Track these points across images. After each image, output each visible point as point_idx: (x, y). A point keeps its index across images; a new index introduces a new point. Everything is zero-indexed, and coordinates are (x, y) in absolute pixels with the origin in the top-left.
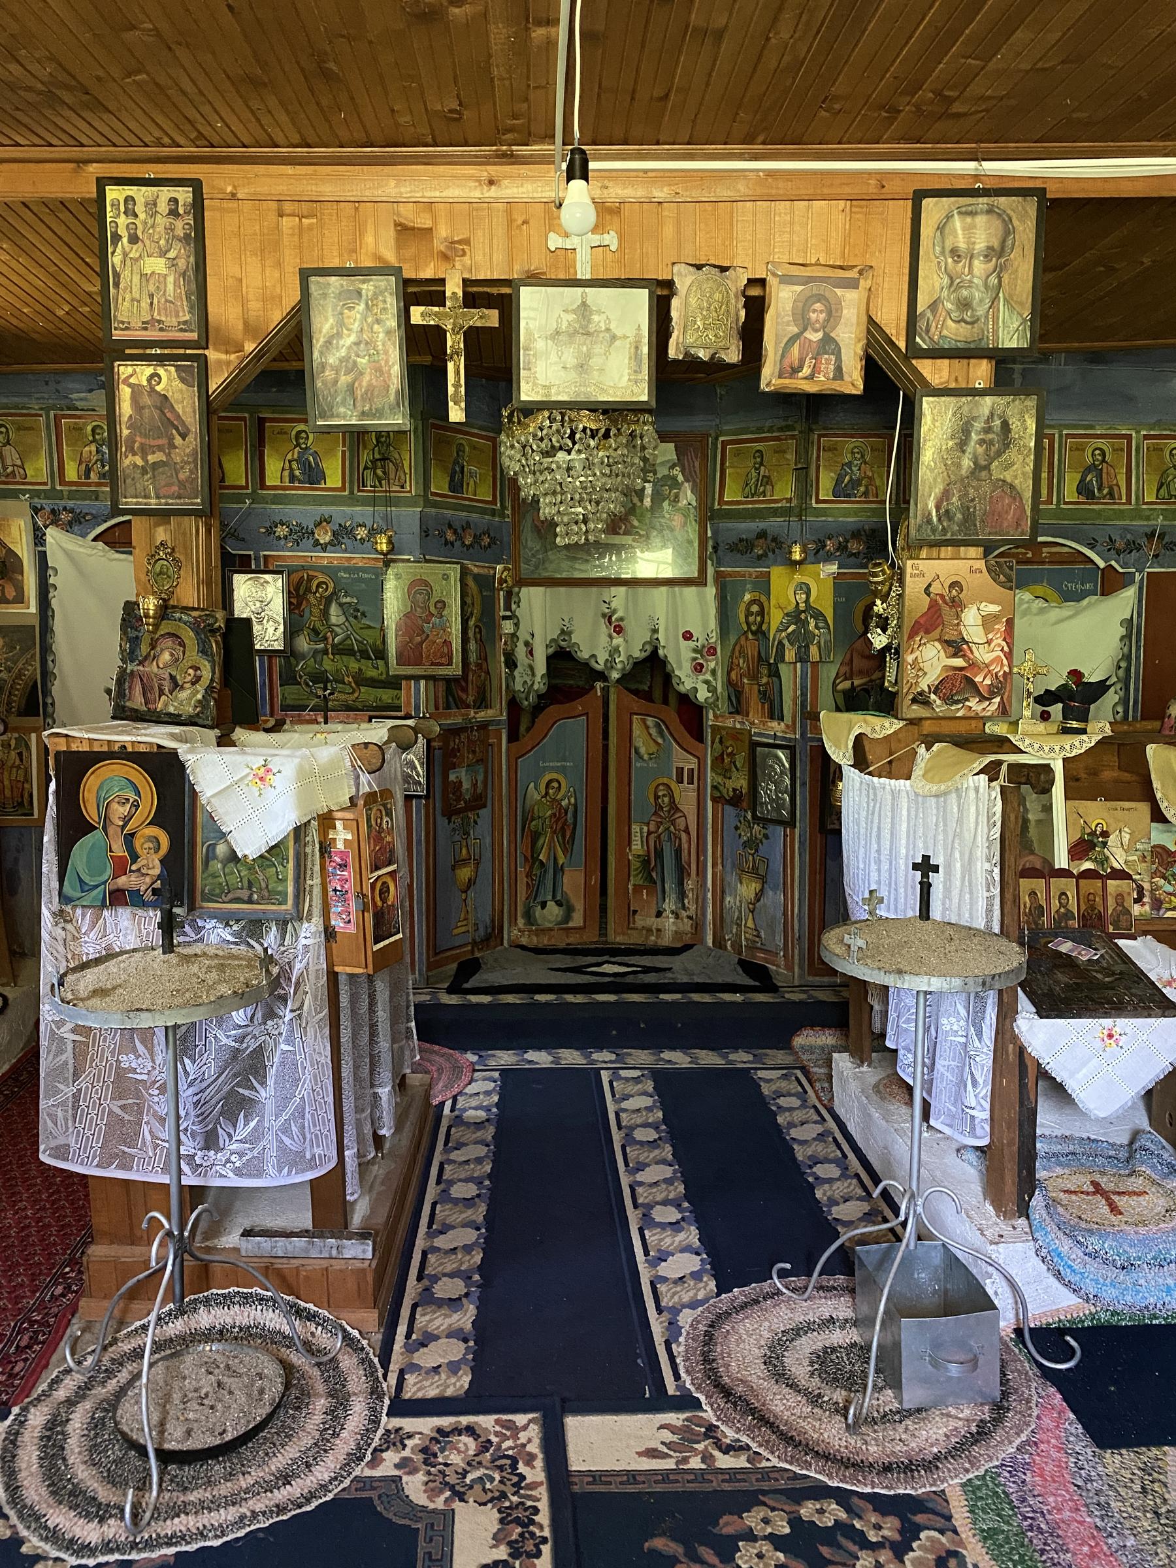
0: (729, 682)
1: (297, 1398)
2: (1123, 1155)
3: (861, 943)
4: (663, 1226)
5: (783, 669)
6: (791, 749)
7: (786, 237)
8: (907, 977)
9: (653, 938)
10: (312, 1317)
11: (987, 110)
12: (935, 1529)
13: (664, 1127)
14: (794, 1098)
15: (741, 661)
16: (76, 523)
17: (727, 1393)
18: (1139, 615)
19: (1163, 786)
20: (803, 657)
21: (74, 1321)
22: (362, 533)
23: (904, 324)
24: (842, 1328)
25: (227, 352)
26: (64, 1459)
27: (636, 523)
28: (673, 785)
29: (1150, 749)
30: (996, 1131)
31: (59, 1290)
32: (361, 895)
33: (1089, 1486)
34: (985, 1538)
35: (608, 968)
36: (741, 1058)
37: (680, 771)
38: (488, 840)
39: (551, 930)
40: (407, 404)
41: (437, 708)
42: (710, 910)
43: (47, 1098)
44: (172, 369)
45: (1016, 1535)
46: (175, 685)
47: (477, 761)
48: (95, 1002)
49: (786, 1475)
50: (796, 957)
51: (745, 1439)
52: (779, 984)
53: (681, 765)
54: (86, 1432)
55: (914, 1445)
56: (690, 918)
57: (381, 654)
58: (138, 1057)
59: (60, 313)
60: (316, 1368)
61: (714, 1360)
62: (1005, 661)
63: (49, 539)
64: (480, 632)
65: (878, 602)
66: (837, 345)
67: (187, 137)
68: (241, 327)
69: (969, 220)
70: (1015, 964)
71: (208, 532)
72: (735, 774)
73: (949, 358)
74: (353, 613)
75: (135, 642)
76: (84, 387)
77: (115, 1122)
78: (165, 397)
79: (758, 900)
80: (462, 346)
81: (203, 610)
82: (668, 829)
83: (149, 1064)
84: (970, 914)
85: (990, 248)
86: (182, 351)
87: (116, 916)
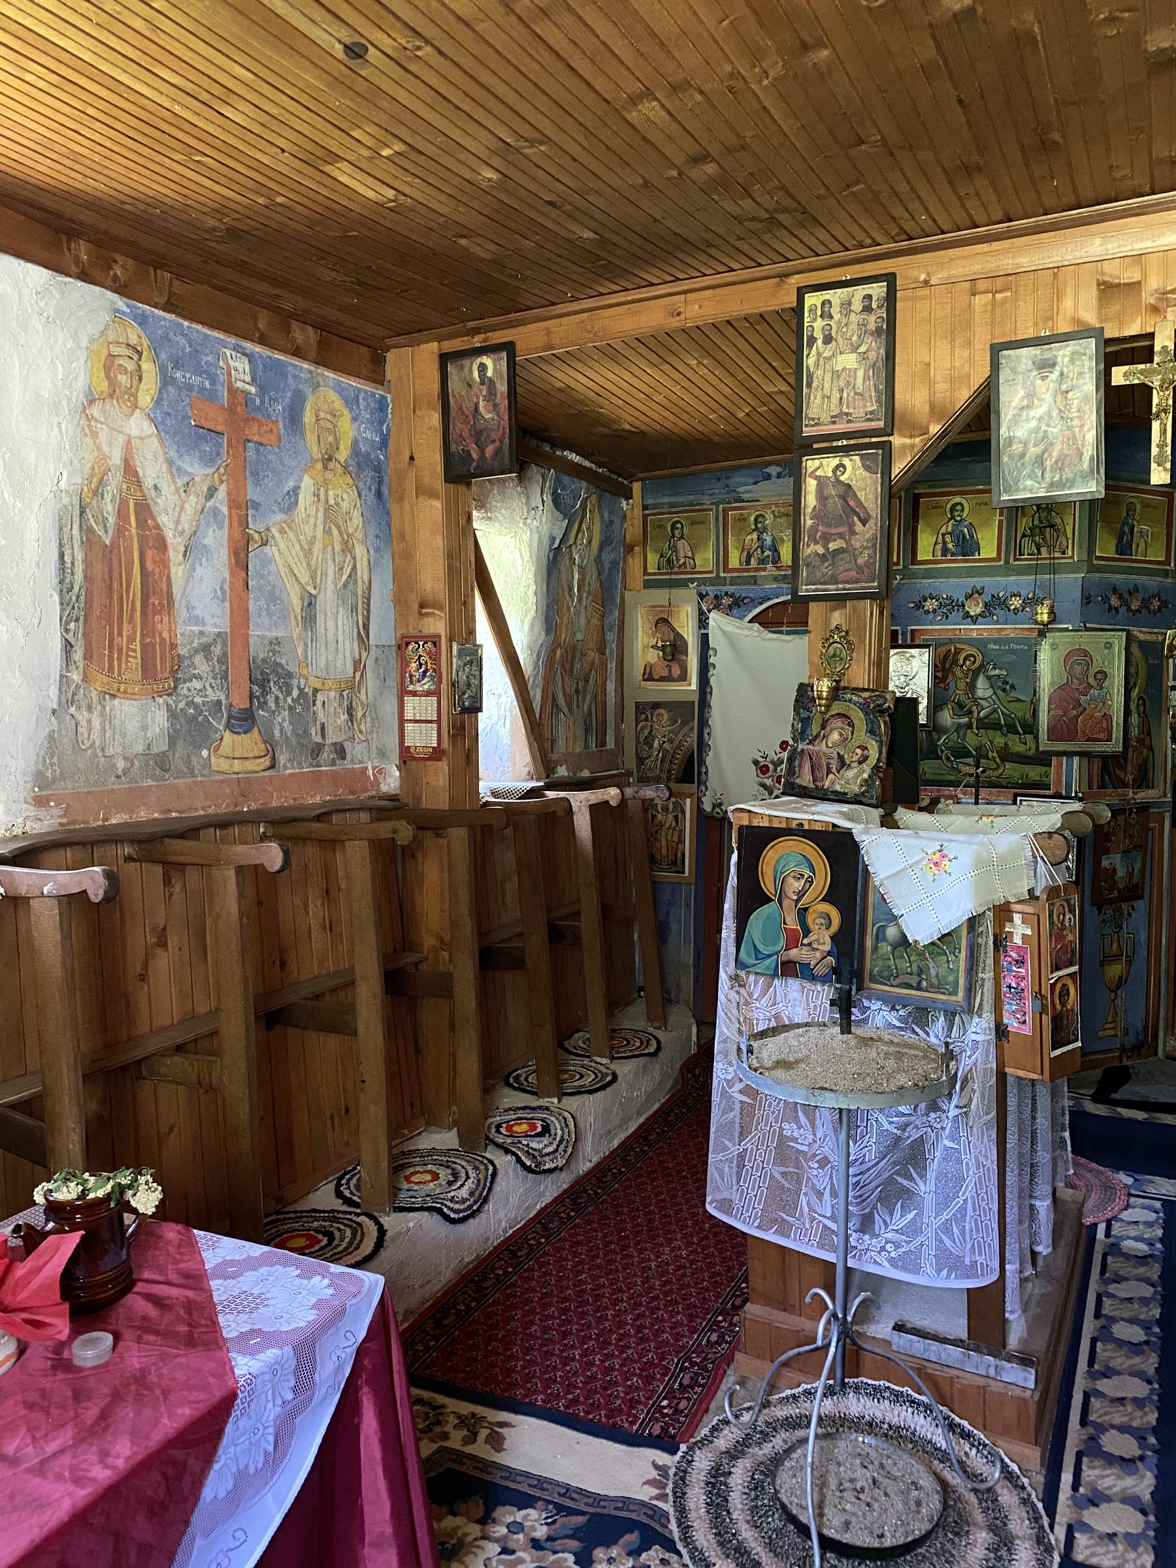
1: (955, 1522)
4: (1120, 1343)
10: (965, 1435)
13: (1157, 1330)
16: (736, 606)
21: (728, 1372)
22: (1016, 603)
25: (911, 437)
26: (728, 1512)
31: (714, 1337)
32: (1038, 995)
38: (1143, 936)
40: (1102, 470)
41: (1091, 787)
43: (716, 1152)
44: (857, 458)
46: (842, 764)
47: (1135, 847)
48: (779, 1073)
54: (747, 1490)
57: (1031, 728)
58: (800, 1127)
59: (741, 415)
60: (972, 1494)
63: (711, 622)
67: (887, 233)
68: (927, 409)
71: (881, 613)
74: (1002, 686)
75: (806, 722)
76: (751, 480)
77: (775, 1188)
78: (849, 486)
80: (1170, 402)
81: (873, 691)
83: (817, 1138)
86: (867, 440)
87: (786, 986)
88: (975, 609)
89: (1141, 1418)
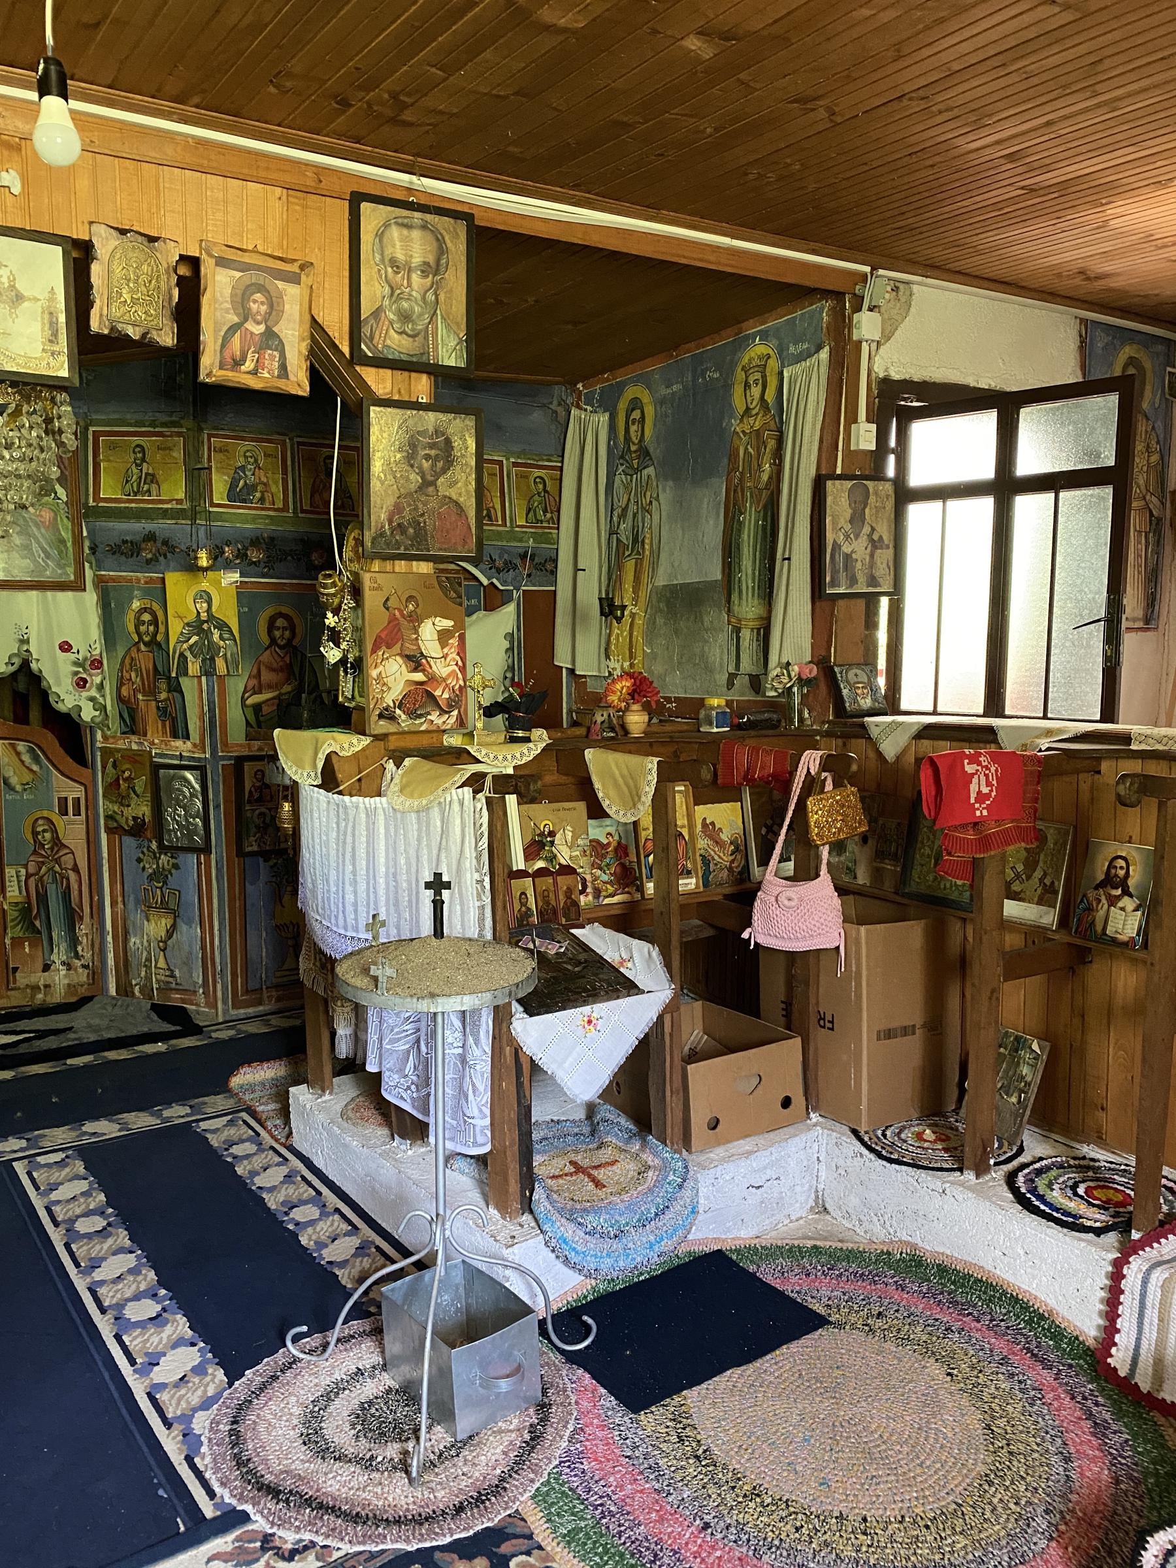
0: (120, 698)
2: (586, 1130)
3: (390, 972)
4: (89, 1236)
5: (185, 683)
6: (200, 769)
7: (219, 216)
8: (440, 1000)
9: (40, 996)
11: (435, 125)
12: (522, 1553)
13: (111, 1210)
14: (247, 1144)
15: (133, 675)
17: (274, 1492)
18: (519, 630)
19: (603, 785)
20: (209, 670)
23: (346, 328)
24: (372, 1377)
28: (55, 818)
29: (589, 754)
30: (497, 1134)
33: (637, 1453)
34: (569, 1543)
36: (177, 1113)
37: (63, 802)
42: (111, 956)
45: (593, 1527)
49: (362, 1558)
50: (219, 994)
51: (307, 1536)
53: (63, 795)
55: (477, 1474)
56: (83, 966)
61: (249, 1460)
62: (460, 675)
65: (329, 615)
66: (281, 341)
69: (405, 232)
70: (530, 970)
73: (392, 369)
84: (462, 925)
85: (426, 263)
89: (212, 1380)
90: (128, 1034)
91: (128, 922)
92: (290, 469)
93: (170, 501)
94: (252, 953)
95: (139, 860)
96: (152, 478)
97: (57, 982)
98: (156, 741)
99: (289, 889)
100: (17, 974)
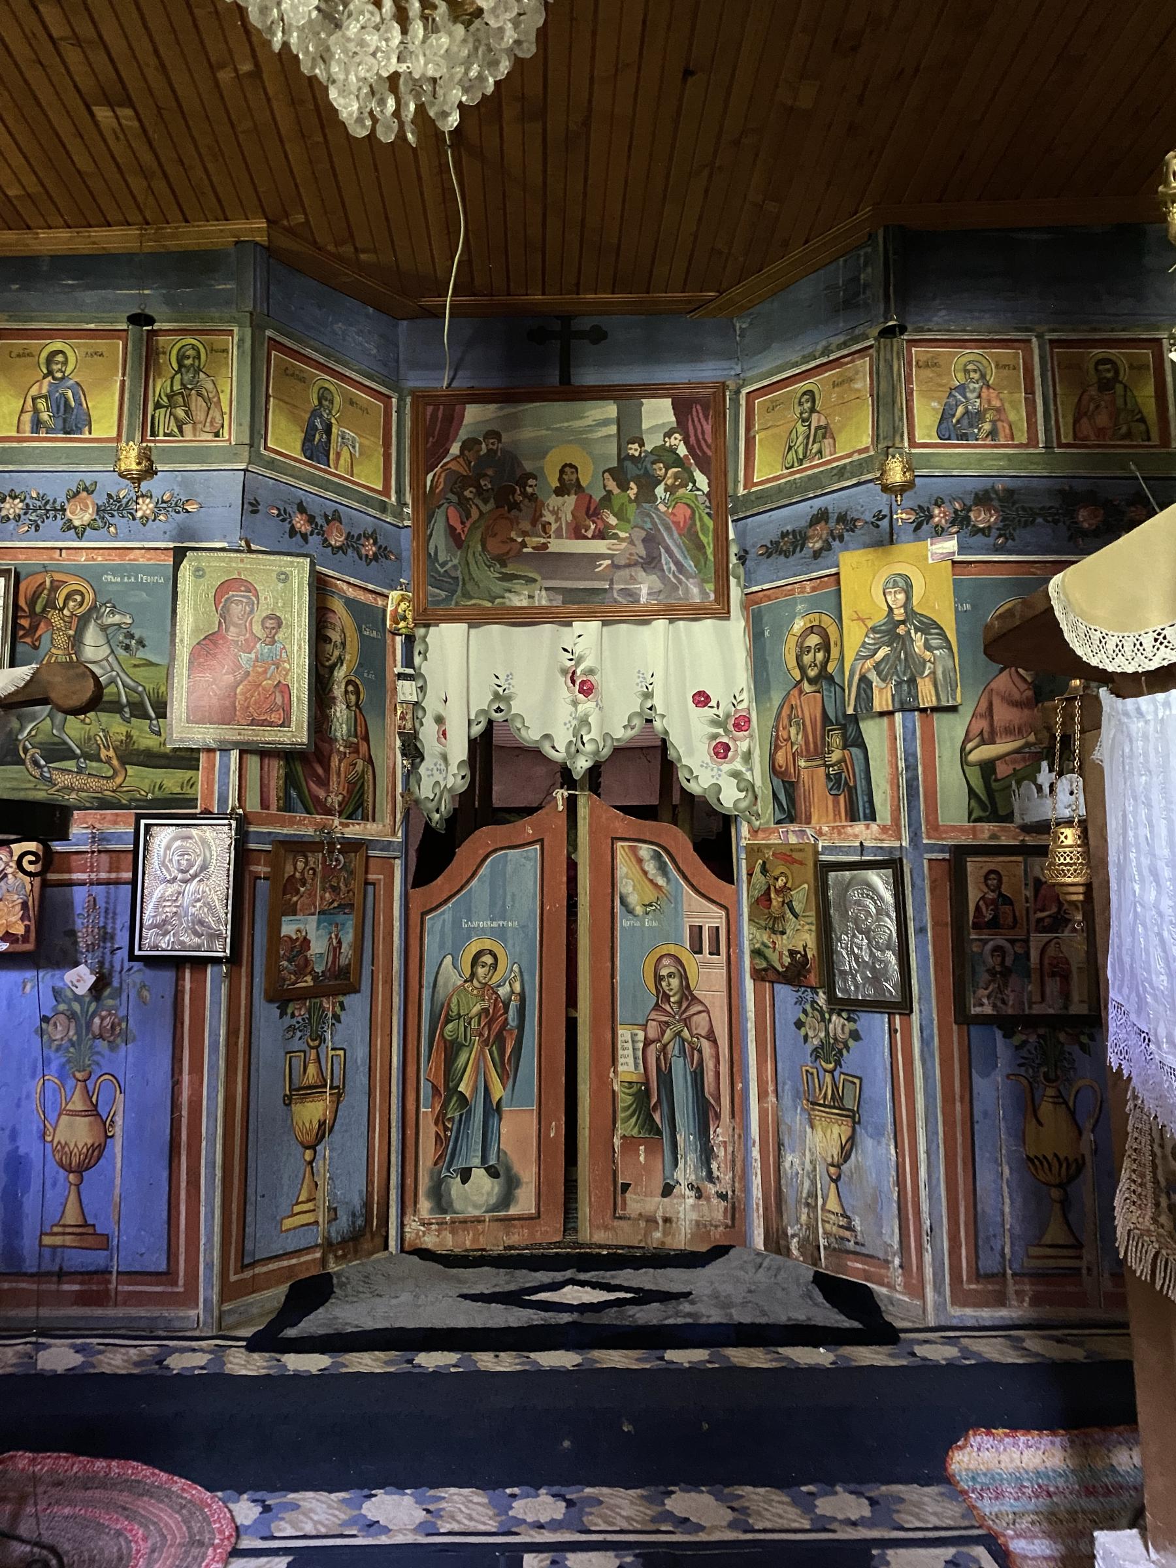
0: (774, 770)
5: (872, 731)
6: (892, 864)
9: (657, 1235)
15: (793, 731)
27: (613, 521)
28: (686, 956)
35: (573, 1295)
37: (697, 931)
39: (479, 1220)
52: (899, 1324)
56: (722, 1196)
64: (357, 692)
72: (791, 923)
74: (127, 641)
79: (847, 1158)
82: (678, 1034)
88: (81, 515)
90: (771, 1320)
91: (783, 1127)
92: (1038, 381)
93: (850, 455)
94: (987, 1204)
95: (799, 1024)
96: (825, 431)
97: (682, 1215)
98: (825, 829)
99: (1050, 1092)
100: (627, 1195)
